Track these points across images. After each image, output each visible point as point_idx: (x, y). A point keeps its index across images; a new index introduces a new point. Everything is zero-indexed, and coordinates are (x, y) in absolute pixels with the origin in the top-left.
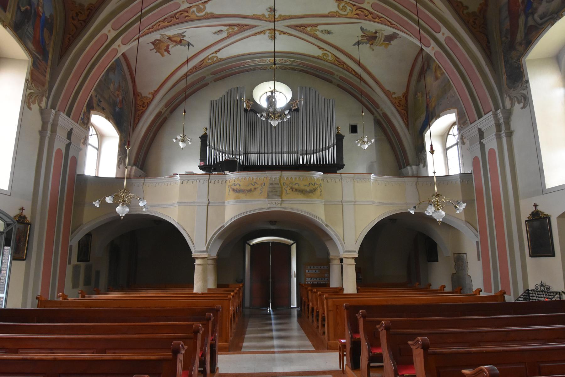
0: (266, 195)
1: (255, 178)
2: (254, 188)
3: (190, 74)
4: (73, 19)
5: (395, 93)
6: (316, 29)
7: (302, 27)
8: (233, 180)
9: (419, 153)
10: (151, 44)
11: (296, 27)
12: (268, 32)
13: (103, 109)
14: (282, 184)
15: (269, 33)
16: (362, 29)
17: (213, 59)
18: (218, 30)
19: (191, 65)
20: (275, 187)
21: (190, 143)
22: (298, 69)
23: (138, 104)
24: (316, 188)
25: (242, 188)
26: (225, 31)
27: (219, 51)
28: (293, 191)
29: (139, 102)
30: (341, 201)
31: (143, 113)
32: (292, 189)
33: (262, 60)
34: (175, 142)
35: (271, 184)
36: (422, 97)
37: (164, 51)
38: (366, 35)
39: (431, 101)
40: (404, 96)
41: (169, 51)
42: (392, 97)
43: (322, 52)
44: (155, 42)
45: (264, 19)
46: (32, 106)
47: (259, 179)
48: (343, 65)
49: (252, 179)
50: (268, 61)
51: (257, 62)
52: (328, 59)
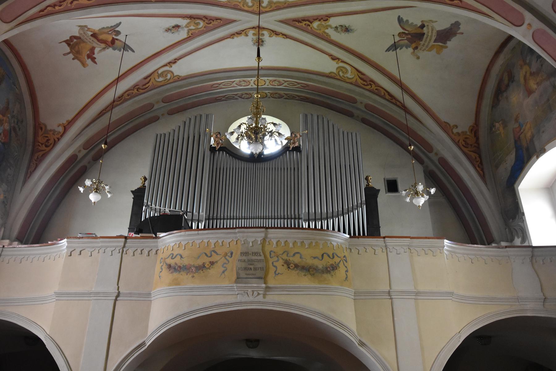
0: (234, 277)
1: (213, 241)
2: (210, 262)
3: (128, 97)
6: (327, 24)
7: (305, 22)
8: (169, 247)
9: (511, 220)
10: (64, 44)
11: (295, 22)
12: (251, 32)
15: (254, 34)
16: (400, 20)
17: (166, 76)
18: (173, 24)
20: (252, 260)
21: (109, 196)
22: (299, 96)
24: (337, 263)
25: (186, 262)
26: (183, 28)
27: (175, 61)
28: (289, 268)
29: (40, 139)
31: (45, 155)
32: (287, 263)
33: (244, 81)
34: (82, 192)
36: (503, 129)
37: (86, 58)
38: (407, 32)
39: (524, 130)
41: (95, 58)
42: (453, 133)
43: (337, 66)
44: (72, 42)
45: (246, 8)
47: (221, 244)
48: (371, 85)
49: (206, 245)
50: (252, 82)
51: (236, 85)
52: (347, 77)
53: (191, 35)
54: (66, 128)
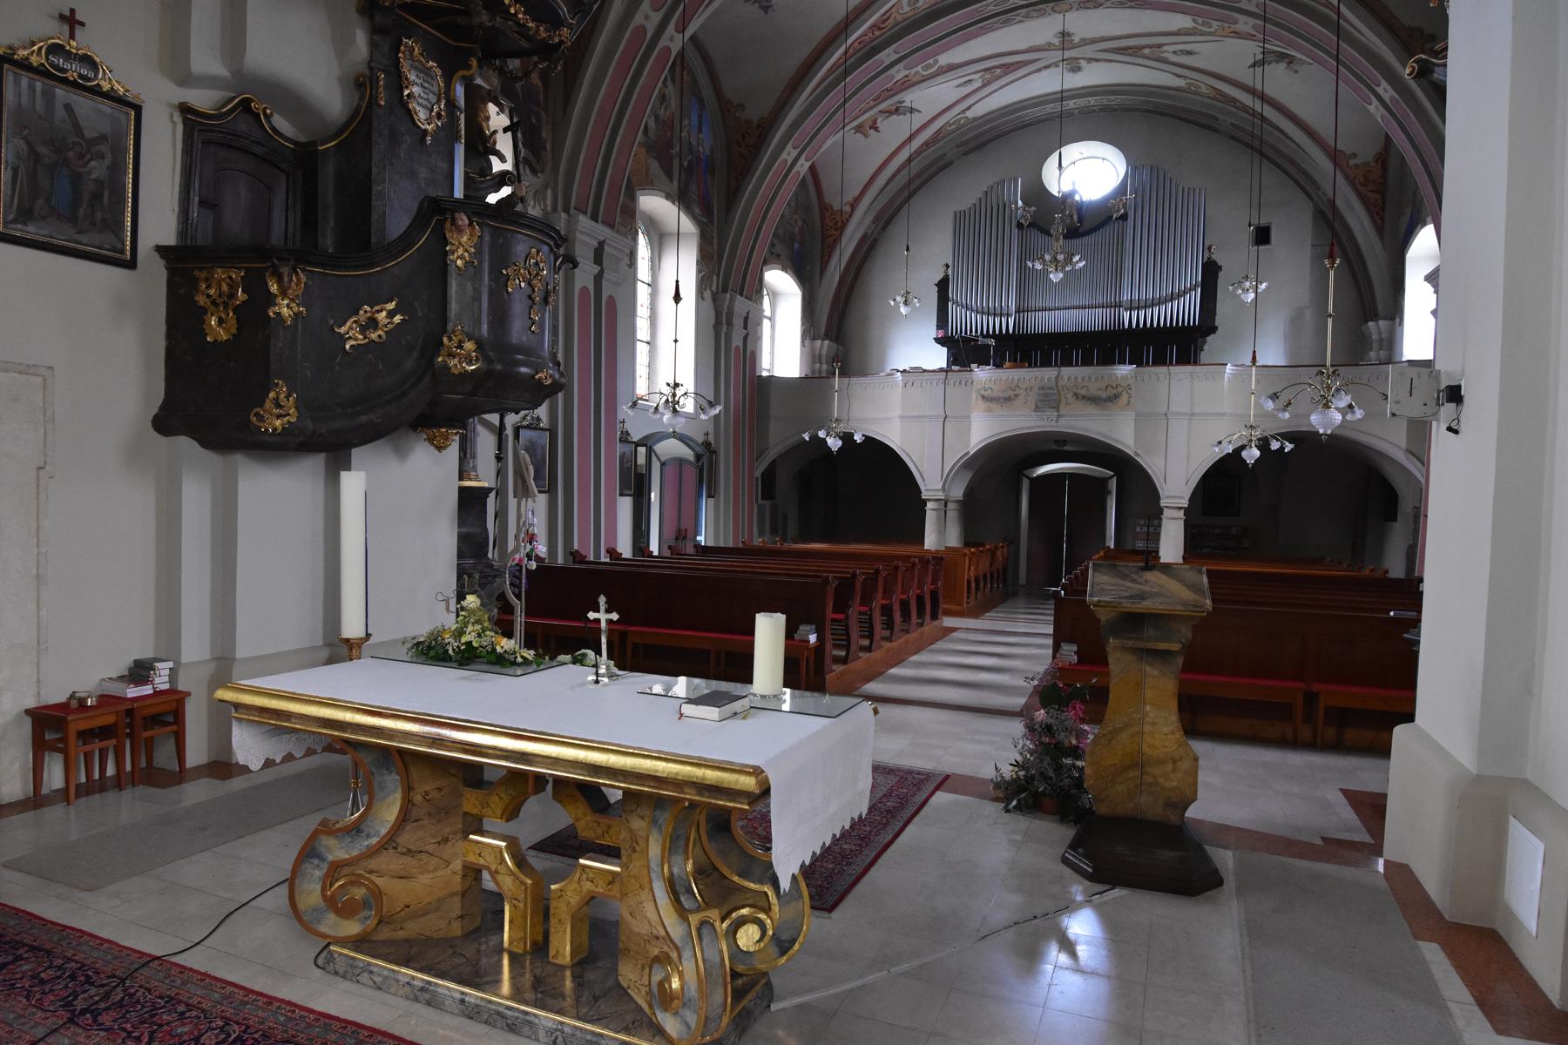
0: (1033, 407)
1: (1016, 378)
4: (740, 146)
5: (1355, 155)
13: (778, 256)
14: (1060, 388)
19: (917, 143)
21: (918, 305)
25: (996, 394)
27: (969, 108)
30: (1166, 414)
32: (1076, 395)
35: (1042, 388)
40: (1377, 161)
42: (1348, 165)
43: (1185, 82)
54: (854, 204)
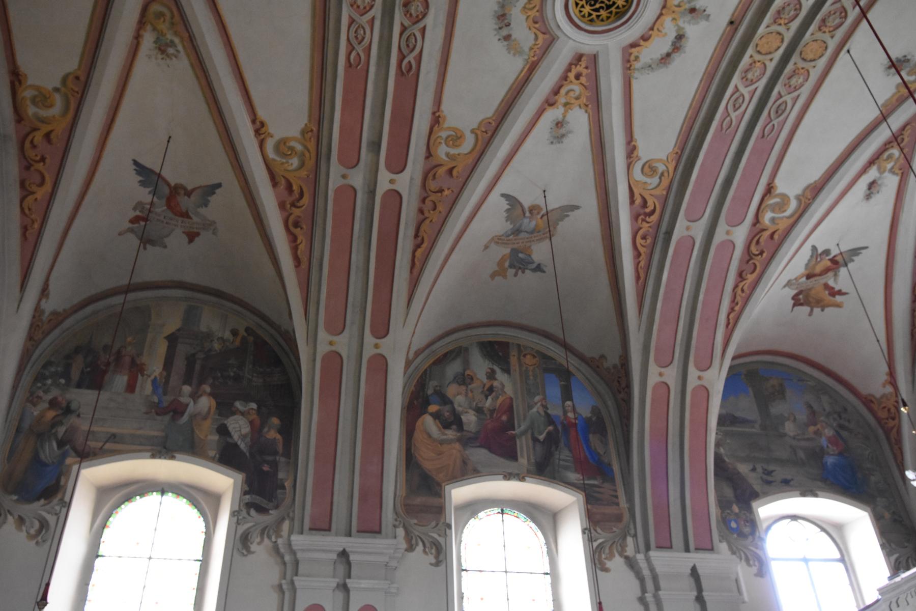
10: (796, 308)
13: (786, 482)
23: (883, 419)
37: (831, 298)
46: (609, 564)
53: (901, 171)
